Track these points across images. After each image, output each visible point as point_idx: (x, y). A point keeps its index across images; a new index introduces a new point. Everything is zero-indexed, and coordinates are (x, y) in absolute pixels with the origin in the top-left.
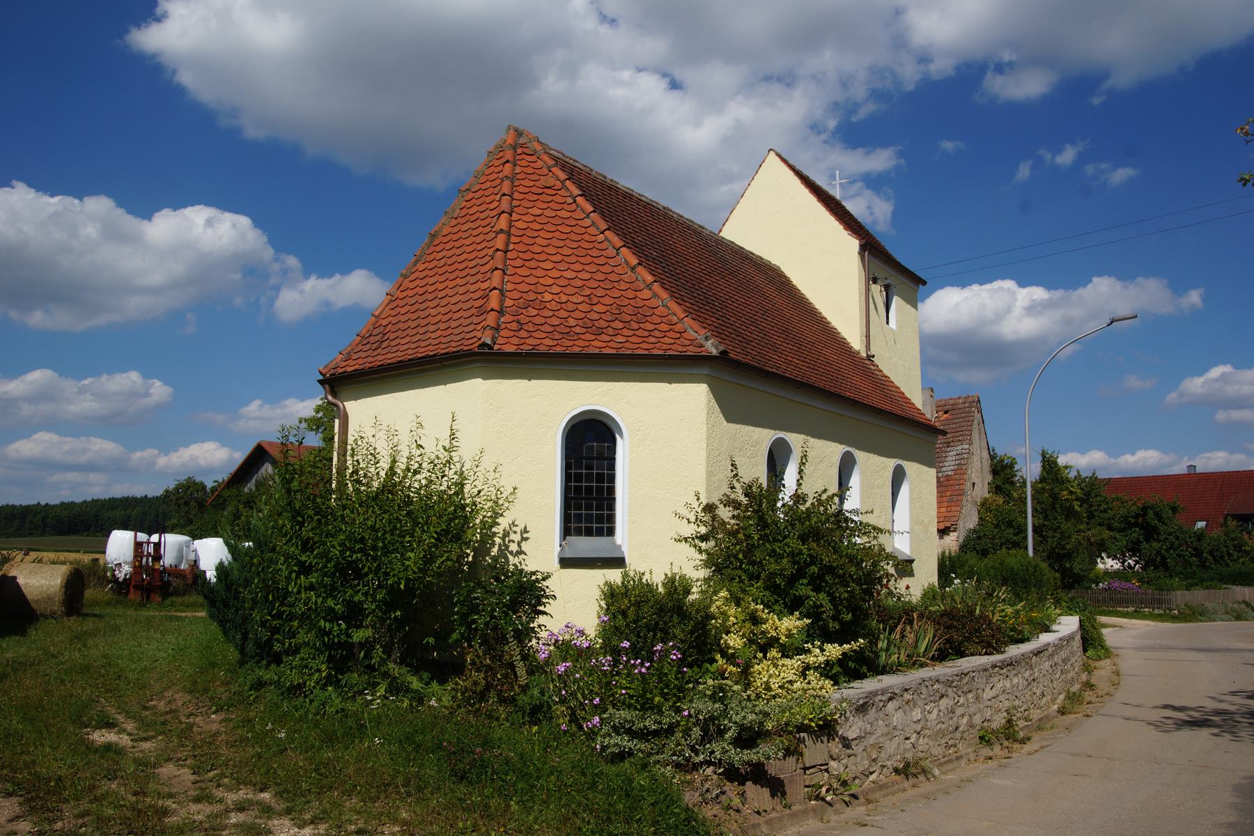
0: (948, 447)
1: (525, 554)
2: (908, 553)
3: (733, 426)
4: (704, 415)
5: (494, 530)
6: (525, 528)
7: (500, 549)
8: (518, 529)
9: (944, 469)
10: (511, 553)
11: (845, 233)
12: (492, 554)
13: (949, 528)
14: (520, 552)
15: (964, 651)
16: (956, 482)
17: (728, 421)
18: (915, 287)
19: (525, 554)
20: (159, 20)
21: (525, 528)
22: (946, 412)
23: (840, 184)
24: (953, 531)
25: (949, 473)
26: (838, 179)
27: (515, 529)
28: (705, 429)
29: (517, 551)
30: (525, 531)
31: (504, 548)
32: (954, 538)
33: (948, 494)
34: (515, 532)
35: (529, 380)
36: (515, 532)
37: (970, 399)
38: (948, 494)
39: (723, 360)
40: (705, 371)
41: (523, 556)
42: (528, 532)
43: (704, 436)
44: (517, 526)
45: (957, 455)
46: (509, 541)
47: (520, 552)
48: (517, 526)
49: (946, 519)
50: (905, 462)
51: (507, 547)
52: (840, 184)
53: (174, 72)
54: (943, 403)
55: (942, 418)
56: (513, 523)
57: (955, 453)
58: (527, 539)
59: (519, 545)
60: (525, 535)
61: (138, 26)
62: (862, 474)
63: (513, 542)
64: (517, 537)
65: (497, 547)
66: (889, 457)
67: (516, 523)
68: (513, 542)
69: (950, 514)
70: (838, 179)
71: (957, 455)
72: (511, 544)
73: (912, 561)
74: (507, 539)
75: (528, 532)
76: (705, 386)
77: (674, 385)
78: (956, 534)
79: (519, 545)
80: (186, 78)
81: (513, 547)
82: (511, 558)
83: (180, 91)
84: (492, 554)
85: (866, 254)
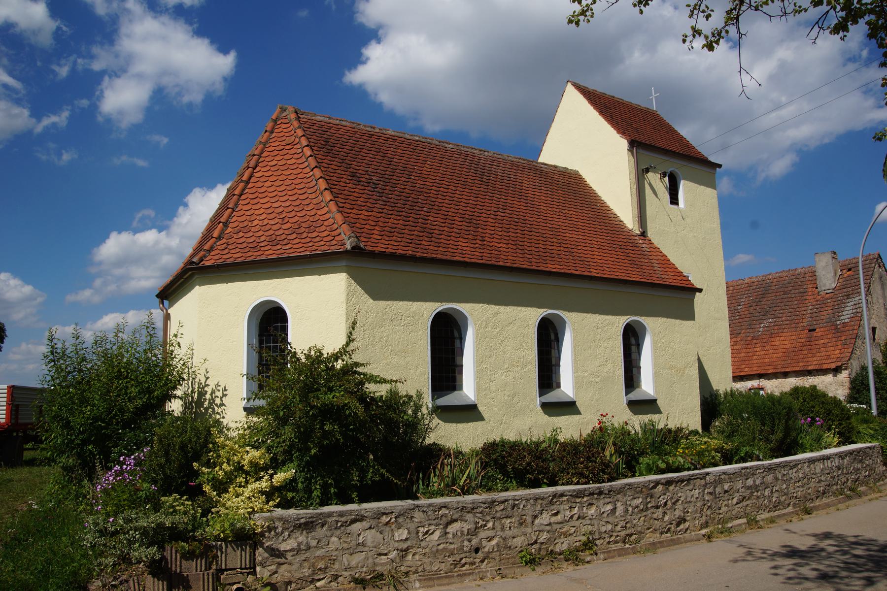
0: (847, 299)
1: (225, 406)
2: (571, 396)
3: (382, 304)
4: (343, 297)
5: (206, 389)
6: (225, 387)
7: (209, 403)
8: (220, 388)
9: (842, 318)
10: (216, 405)
11: (618, 136)
12: (205, 406)
13: (840, 367)
14: (222, 405)
15: (557, 481)
16: (851, 328)
17: (374, 299)
18: (712, 171)
19: (225, 406)
20: (364, 63)
21: (225, 387)
22: (849, 270)
23: (652, 95)
24: (844, 370)
25: (846, 321)
26: (653, 94)
27: (218, 388)
28: (345, 307)
29: (220, 404)
30: (225, 390)
31: (212, 402)
32: (846, 375)
33: (843, 338)
34: (219, 391)
35: (320, 275)
36: (219, 391)
37: (871, 257)
38: (843, 338)
39: (357, 252)
40: (344, 263)
41: (223, 407)
42: (226, 390)
43: (344, 312)
44: (220, 386)
45: (855, 305)
46: (216, 397)
47: (222, 405)
48: (220, 386)
49: (839, 359)
50: (643, 318)
51: (214, 401)
52: (652, 95)
53: (376, 95)
54: (847, 262)
55: (845, 275)
56: (217, 384)
57: (852, 303)
58: (226, 395)
59: (222, 400)
60: (225, 393)
61: (350, 69)
62: (574, 330)
63: (218, 397)
64: (219, 394)
65: (208, 401)
66: (618, 315)
67: (219, 384)
68: (218, 397)
69: (842, 355)
70: (653, 94)
71: (855, 305)
72: (216, 399)
73: (655, 400)
74: (214, 395)
75: (226, 390)
76: (345, 274)
77: (322, 276)
78: (847, 372)
79: (222, 400)
80: (385, 98)
81: (218, 401)
82: (216, 408)
83: (379, 106)
84: (205, 406)
85: (635, 150)
